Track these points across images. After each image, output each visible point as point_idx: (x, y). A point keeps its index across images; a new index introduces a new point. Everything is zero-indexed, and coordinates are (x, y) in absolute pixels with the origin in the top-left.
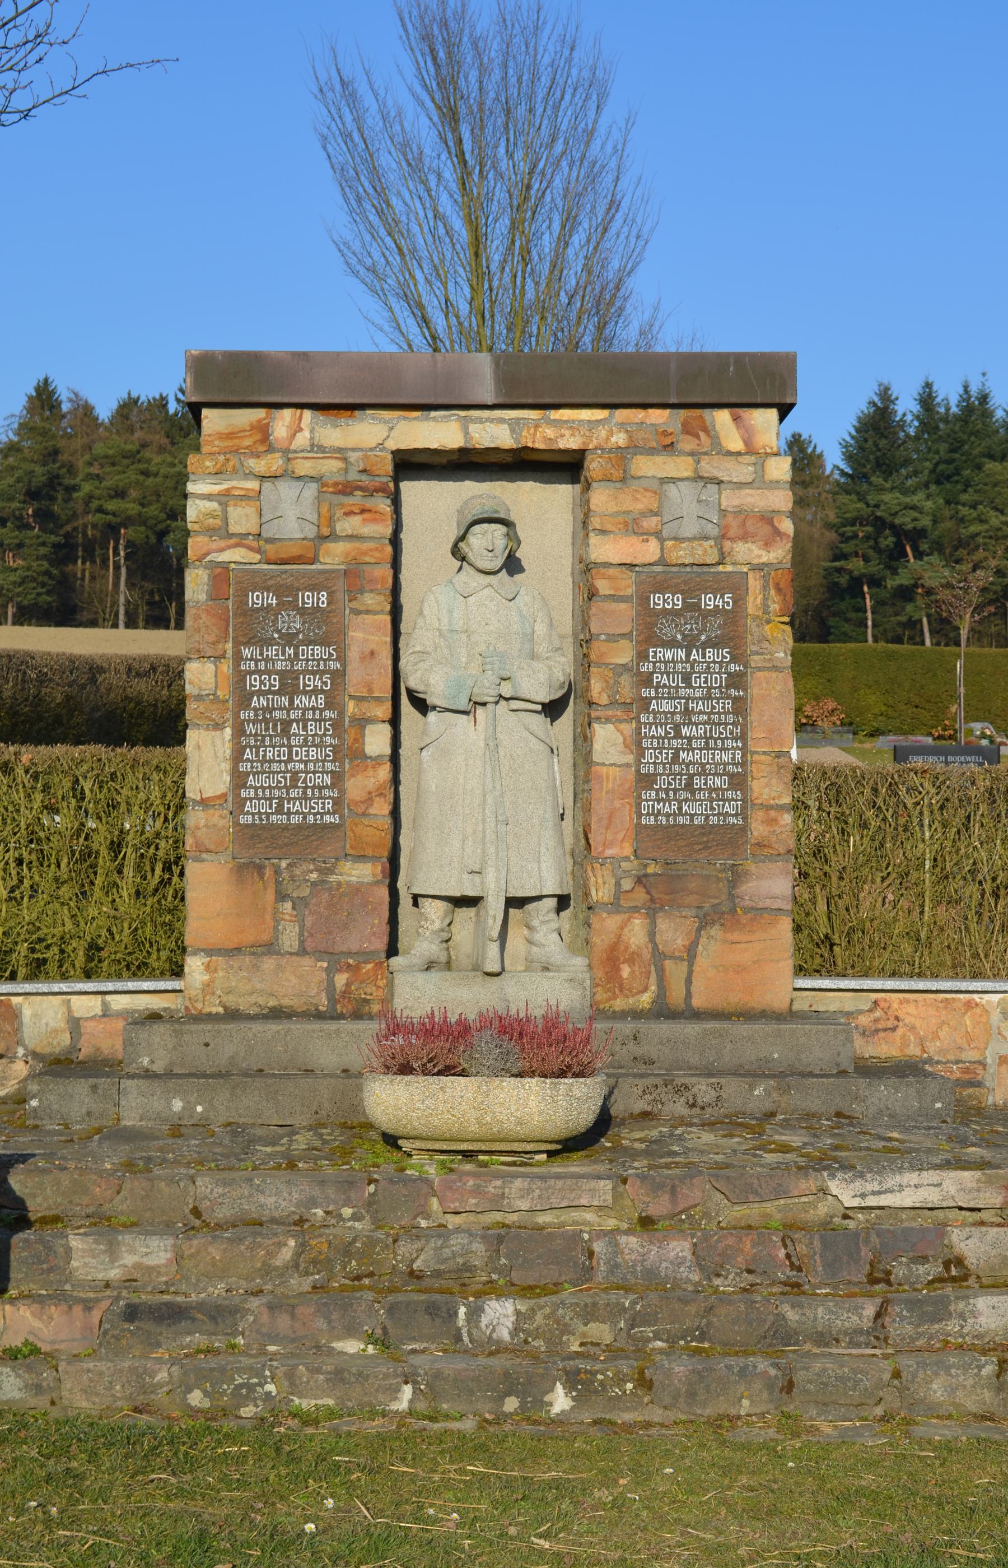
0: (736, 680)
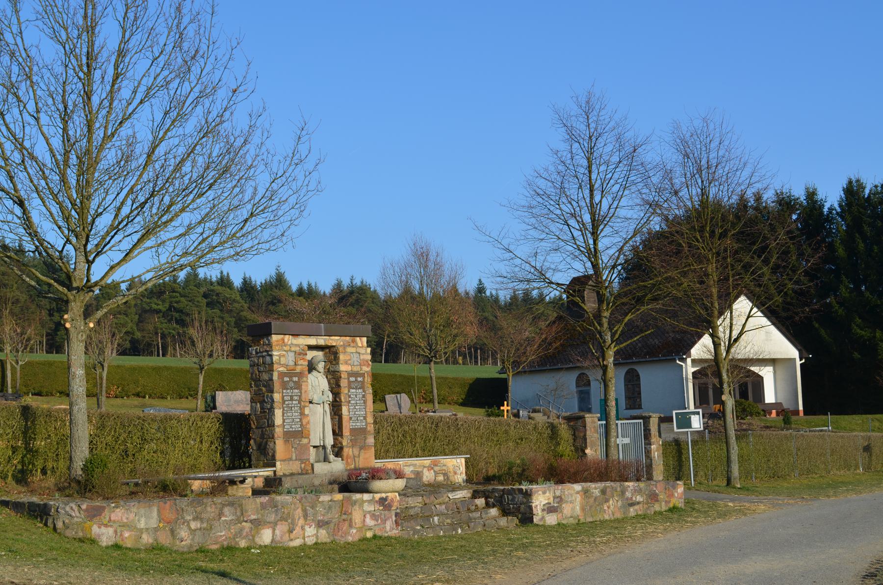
0: (364, 396)
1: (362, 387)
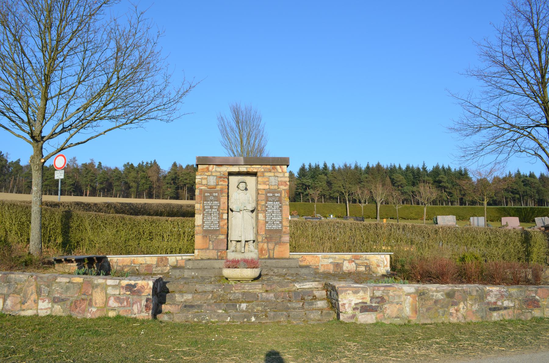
0: (280, 207)
1: (280, 200)
